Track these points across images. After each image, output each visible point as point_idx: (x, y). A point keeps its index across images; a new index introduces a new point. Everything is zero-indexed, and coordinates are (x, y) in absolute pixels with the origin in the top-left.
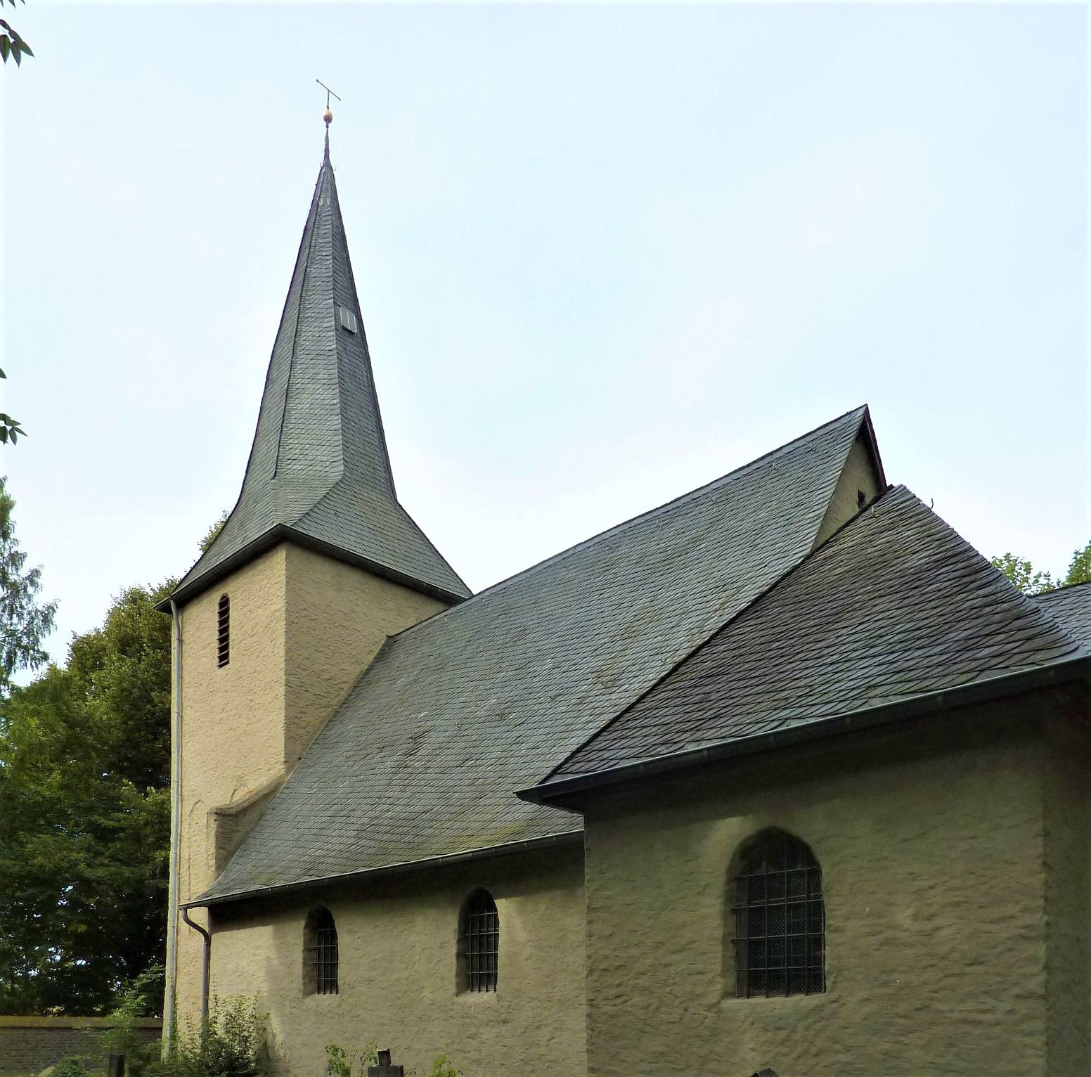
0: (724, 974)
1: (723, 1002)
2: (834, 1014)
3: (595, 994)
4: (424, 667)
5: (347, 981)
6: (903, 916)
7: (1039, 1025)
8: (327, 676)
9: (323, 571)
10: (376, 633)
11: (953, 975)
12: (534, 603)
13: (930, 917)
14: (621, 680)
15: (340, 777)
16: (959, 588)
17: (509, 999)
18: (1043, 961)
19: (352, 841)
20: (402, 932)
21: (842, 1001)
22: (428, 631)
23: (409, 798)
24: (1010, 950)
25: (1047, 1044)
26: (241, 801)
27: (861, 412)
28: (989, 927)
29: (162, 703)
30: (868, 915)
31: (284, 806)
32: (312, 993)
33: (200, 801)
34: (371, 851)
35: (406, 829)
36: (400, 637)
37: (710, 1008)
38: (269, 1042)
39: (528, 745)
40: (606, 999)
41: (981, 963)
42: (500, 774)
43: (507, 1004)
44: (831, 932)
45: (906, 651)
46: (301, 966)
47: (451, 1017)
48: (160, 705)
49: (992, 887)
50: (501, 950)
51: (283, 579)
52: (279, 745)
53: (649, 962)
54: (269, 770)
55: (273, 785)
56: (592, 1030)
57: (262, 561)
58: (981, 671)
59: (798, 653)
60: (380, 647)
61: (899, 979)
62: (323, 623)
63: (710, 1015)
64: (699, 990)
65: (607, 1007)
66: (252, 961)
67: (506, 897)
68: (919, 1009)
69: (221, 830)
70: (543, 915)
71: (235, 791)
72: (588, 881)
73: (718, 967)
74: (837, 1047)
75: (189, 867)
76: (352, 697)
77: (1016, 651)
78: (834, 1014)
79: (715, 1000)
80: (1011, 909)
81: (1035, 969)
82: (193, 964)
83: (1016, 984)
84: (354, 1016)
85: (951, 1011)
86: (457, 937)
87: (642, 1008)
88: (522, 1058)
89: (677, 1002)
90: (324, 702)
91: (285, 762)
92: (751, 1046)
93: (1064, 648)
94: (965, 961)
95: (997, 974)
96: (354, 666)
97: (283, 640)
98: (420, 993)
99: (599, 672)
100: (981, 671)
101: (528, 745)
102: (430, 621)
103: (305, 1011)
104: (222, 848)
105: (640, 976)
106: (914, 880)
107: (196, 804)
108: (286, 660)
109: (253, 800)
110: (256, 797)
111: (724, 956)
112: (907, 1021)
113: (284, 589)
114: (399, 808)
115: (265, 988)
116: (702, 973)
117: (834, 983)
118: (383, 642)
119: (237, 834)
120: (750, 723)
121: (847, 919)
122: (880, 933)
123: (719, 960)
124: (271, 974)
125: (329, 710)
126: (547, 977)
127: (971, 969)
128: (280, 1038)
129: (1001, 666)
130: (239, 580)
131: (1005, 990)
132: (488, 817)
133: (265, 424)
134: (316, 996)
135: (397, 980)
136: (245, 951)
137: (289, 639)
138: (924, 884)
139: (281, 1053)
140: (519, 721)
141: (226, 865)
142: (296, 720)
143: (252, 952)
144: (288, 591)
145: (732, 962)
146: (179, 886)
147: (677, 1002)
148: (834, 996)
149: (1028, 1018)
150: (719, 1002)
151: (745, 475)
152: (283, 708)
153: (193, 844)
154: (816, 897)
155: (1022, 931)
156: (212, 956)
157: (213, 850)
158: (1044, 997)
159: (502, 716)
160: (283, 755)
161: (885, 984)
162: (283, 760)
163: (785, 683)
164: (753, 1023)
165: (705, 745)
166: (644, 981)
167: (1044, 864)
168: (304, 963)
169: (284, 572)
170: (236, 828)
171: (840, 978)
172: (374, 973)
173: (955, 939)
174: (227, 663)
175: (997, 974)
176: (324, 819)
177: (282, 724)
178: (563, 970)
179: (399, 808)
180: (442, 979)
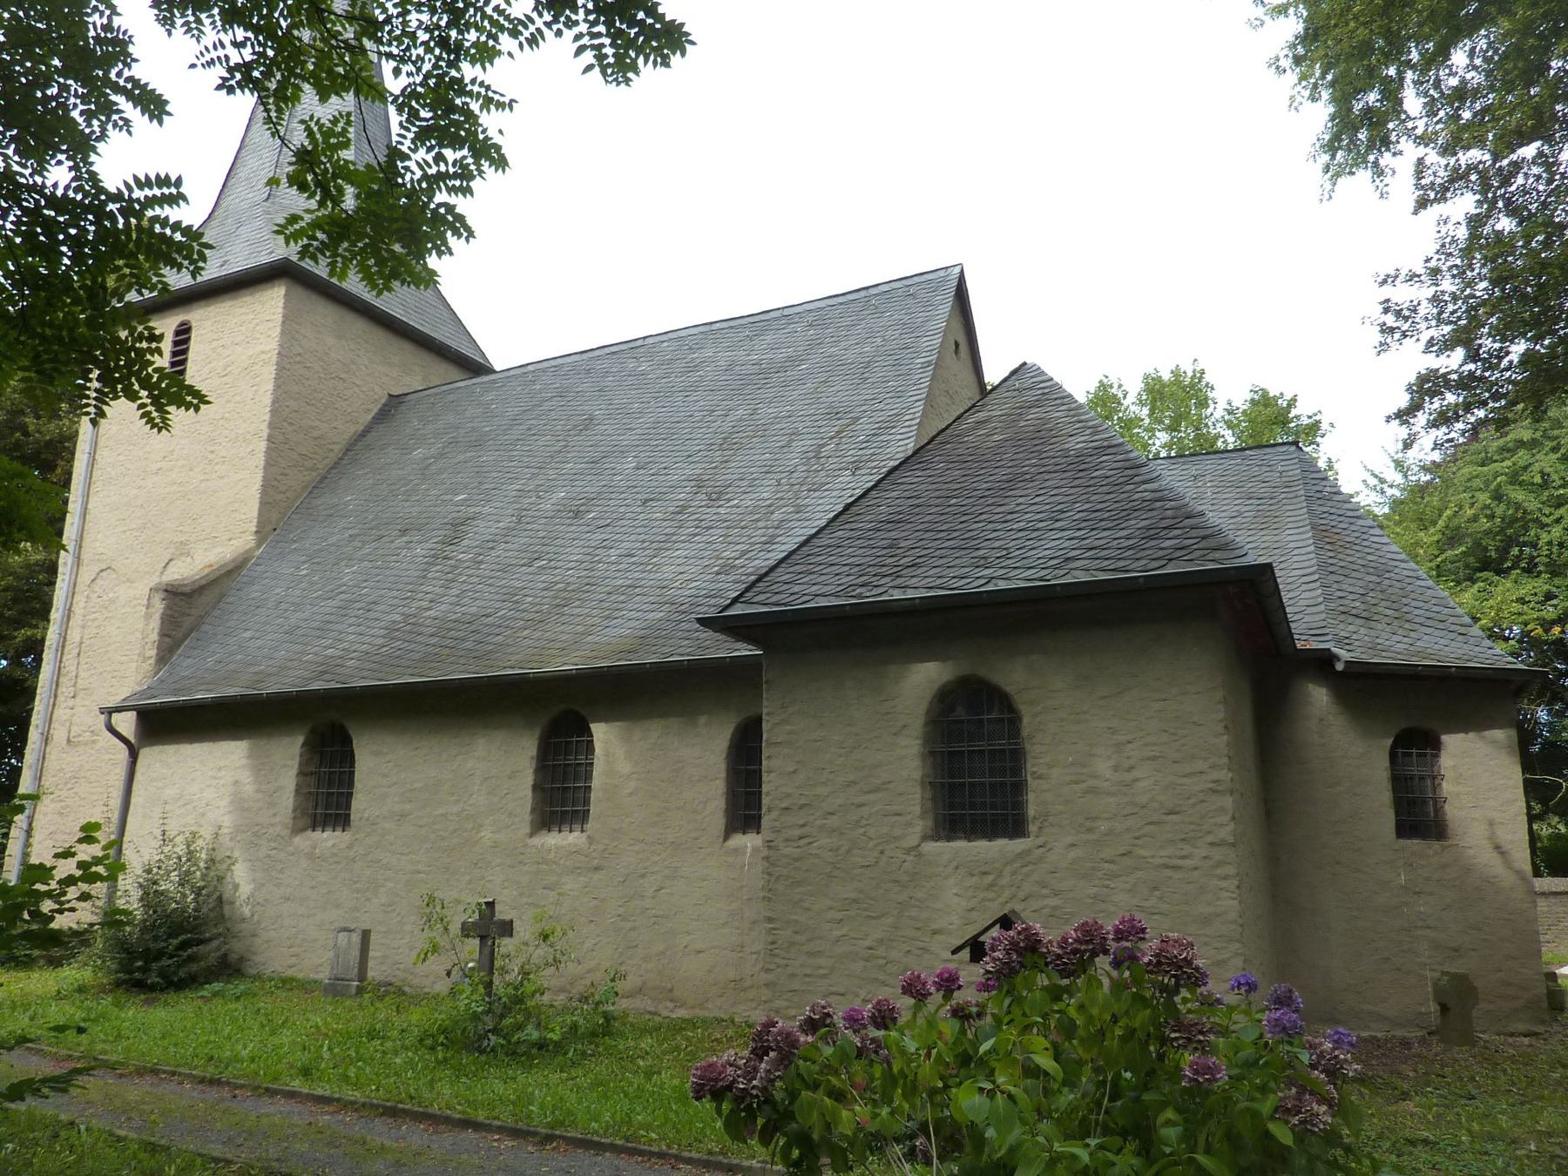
0: (922, 816)
1: (923, 845)
2: (1041, 859)
3: (774, 835)
4: (451, 440)
5: (366, 815)
6: (1103, 767)
7: (1230, 870)
8: (316, 434)
9: (325, 312)
10: (377, 388)
11: (1152, 823)
12: (598, 391)
13: (1131, 768)
14: (727, 493)
15: (344, 559)
16: (1125, 479)
17: (606, 841)
18: (1231, 813)
19: (381, 641)
20: (455, 756)
21: (1049, 847)
22: (451, 397)
23: (457, 596)
24: (1202, 801)
25: (1238, 887)
26: (197, 577)
27: (957, 270)
28: (1184, 780)
29: (40, 433)
30: (1072, 764)
31: (256, 587)
32: (303, 830)
33: (109, 568)
34: (417, 656)
35: (462, 634)
36: (410, 397)
37: (908, 851)
38: (226, 896)
39: (618, 551)
40: (787, 840)
42: (586, 581)
43: (601, 847)
44: (1035, 778)
45: (1093, 529)
46: (293, 794)
47: (520, 862)
48: (37, 435)
49: (1183, 745)
50: (597, 782)
52: (251, 510)
53: (839, 801)
54: (230, 540)
55: (241, 560)
56: (770, 874)
57: (248, 293)
58: (1170, 560)
59: (981, 514)
60: (379, 406)
61: (1103, 826)
62: (318, 372)
63: (910, 858)
64: (897, 832)
65: (788, 849)
66: (209, 786)
67: (600, 721)
68: (1124, 854)
69: (169, 612)
70: (655, 744)
71: (170, 560)
72: (768, 714)
73: (917, 809)
74: (1044, 891)
75: (79, 654)
76: (344, 462)
77: (1195, 547)
78: (1041, 859)
79: (915, 843)
80: (1200, 765)
81: (1225, 819)
82: (69, 786)
83: (1210, 832)
84: (371, 861)
85: (1153, 857)
86: (534, 765)
89: (871, 844)
90: (309, 464)
91: (256, 532)
93: (1237, 551)
94: (1162, 811)
95: (1192, 823)
96: (347, 425)
97: (270, 386)
98: (477, 833)
99: (699, 484)
100: (1170, 560)
101: (618, 551)
102: (450, 386)
103: (292, 854)
104: (169, 636)
105: (828, 816)
106: (1113, 733)
107: (102, 571)
108: (271, 411)
109: (212, 577)
110: (217, 574)
111: (923, 798)
112: (1112, 865)
114: (443, 607)
115: (227, 822)
116: (899, 815)
117: (1040, 828)
118: (383, 401)
119: (186, 618)
120: (954, 577)
121: (1051, 767)
122: (1084, 782)
123: (918, 801)
124: (239, 804)
125: (314, 474)
126: (658, 815)
128: (245, 890)
129: (1185, 558)
130: (210, 309)
131: (1200, 837)
132: (580, 629)
134: (309, 833)
135: (442, 815)
136: (199, 773)
137: (277, 387)
138: (1123, 738)
139: (246, 911)
140: (602, 523)
141: (170, 658)
142: (276, 483)
143: (210, 773)
144: (283, 333)
145: (929, 804)
146: (58, 678)
147: (871, 844)
148: (1040, 841)
149: (1220, 864)
150: (919, 845)
151: (841, 304)
152: (262, 467)
153: (89, 624)
154: (1015, 744)
155: (1211, 785)
156: (138, 777)
157: (154, 636)
158: (1233, 845)
159: (577, 514)
161: (1090, 830)
162: (255, 529)
163: (979, 541)
164: (957, 868)
165: (910, 594)
166: (833, 822)
168: (297, 791)
169: (280, 310)
170: (187, 611)
171: (1046, 824)
172: (408, 806)
173: (1153, 789)
175: (1192, 823)
176: (328, 610)
178: (678, 808)
179: (443, 607)
180: (510, 815)
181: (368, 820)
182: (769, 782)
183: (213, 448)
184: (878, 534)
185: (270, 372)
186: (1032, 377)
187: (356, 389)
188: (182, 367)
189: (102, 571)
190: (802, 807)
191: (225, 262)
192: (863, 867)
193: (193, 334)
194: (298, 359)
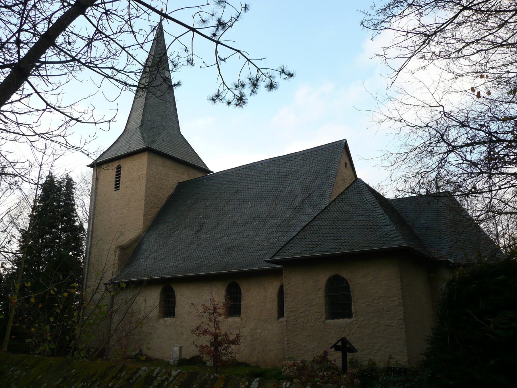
0: (325, 313)
5: (179, 313)
7: (404, 326)
9: (159, 160)
25: (405, 331)
27: (345, 141)
41: (389, 311)
51: (146, 164)
85: (384, 323)
87: (302, 322)
88: (250, 340)
89: (313, 321)
91: (143, 228)
92: (334, 333)
97: (145, 184)
107: (99, 240)
108: (145, 192)
113: (146, 167)
125: (158, 209)
127: (387, 313)
133: (136, 106)
144: (148, 168)
150: (325, 321)
152: (143, 209)
160: (142, 226)
162: (142, 227)
167: (401, 288)
169: (146, 161)
174: (119, 189)
177: (142, 215)
181: (180, 314)
182: (286, 304)
183: (129, 203)
184: (313, 234)
185: (144, 181)
186: (359, 183)
187: (169, 182)
188: (119, 176)
189: (99, 240)
190: (295, 311)
191: (130, 147)
192: (310, 327)
193: (122, 169)
194: (152, 175)
